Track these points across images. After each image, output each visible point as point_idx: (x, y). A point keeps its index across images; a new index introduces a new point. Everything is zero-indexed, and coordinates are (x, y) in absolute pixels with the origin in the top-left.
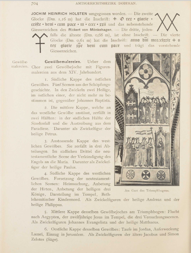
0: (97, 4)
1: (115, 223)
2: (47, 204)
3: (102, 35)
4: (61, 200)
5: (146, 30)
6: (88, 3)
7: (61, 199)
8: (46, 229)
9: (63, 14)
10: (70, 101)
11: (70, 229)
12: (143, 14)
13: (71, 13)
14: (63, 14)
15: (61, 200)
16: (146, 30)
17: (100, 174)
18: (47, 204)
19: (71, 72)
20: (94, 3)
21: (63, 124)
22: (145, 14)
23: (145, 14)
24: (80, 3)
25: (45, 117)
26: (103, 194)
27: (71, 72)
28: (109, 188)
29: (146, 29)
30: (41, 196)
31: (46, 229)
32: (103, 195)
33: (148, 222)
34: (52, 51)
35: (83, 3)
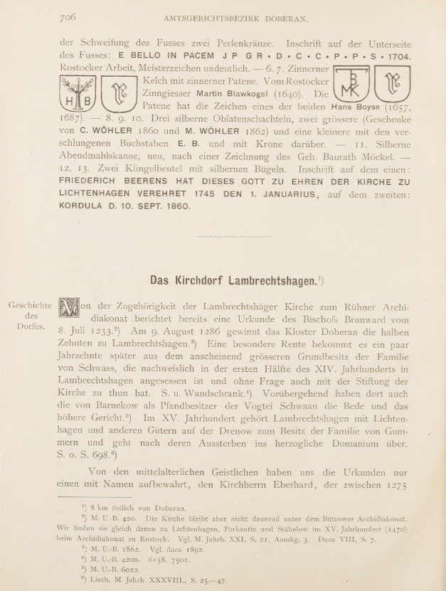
0: (216, 20)
1: (326, 395)
2: (164, 404)
3: (73, 18)
4: (263, 145)
5: (357, 407)
6: (193, 18)
7: (226, 484)
8: (269, 70)
9: (106, 180)
10: (394, 445)
11: (177, 280)
12: (196, 44)
13: (112, 182)
14: (71, 193)
15: (263, 145)
16: (357, 407)
17: (233, 473)
18: (164, 404)
19: (322, 369)
20: (207, 18)
21: (60, 406)
22: (199, 44)
23: (199, 44)
24: (173, 18)
25: (272, 367)
26: (347, 404)
27: (322, 369)
28: (270, 404)
29: (355, 404)
30: (276, 385)
31: (269, 70)
32: (347, 407)
33: (351, 158)
34: (301, 358)
35: (224, 18)
